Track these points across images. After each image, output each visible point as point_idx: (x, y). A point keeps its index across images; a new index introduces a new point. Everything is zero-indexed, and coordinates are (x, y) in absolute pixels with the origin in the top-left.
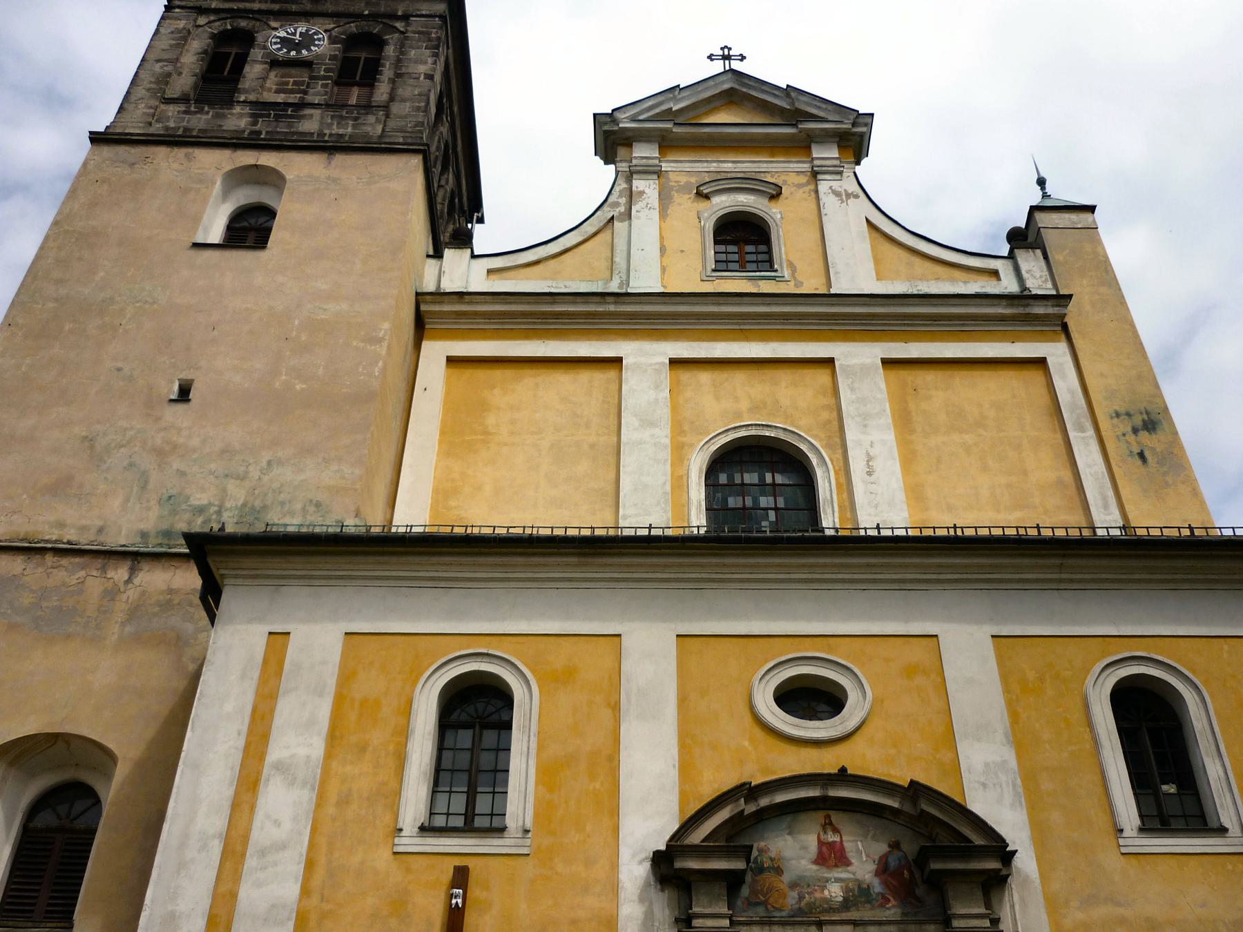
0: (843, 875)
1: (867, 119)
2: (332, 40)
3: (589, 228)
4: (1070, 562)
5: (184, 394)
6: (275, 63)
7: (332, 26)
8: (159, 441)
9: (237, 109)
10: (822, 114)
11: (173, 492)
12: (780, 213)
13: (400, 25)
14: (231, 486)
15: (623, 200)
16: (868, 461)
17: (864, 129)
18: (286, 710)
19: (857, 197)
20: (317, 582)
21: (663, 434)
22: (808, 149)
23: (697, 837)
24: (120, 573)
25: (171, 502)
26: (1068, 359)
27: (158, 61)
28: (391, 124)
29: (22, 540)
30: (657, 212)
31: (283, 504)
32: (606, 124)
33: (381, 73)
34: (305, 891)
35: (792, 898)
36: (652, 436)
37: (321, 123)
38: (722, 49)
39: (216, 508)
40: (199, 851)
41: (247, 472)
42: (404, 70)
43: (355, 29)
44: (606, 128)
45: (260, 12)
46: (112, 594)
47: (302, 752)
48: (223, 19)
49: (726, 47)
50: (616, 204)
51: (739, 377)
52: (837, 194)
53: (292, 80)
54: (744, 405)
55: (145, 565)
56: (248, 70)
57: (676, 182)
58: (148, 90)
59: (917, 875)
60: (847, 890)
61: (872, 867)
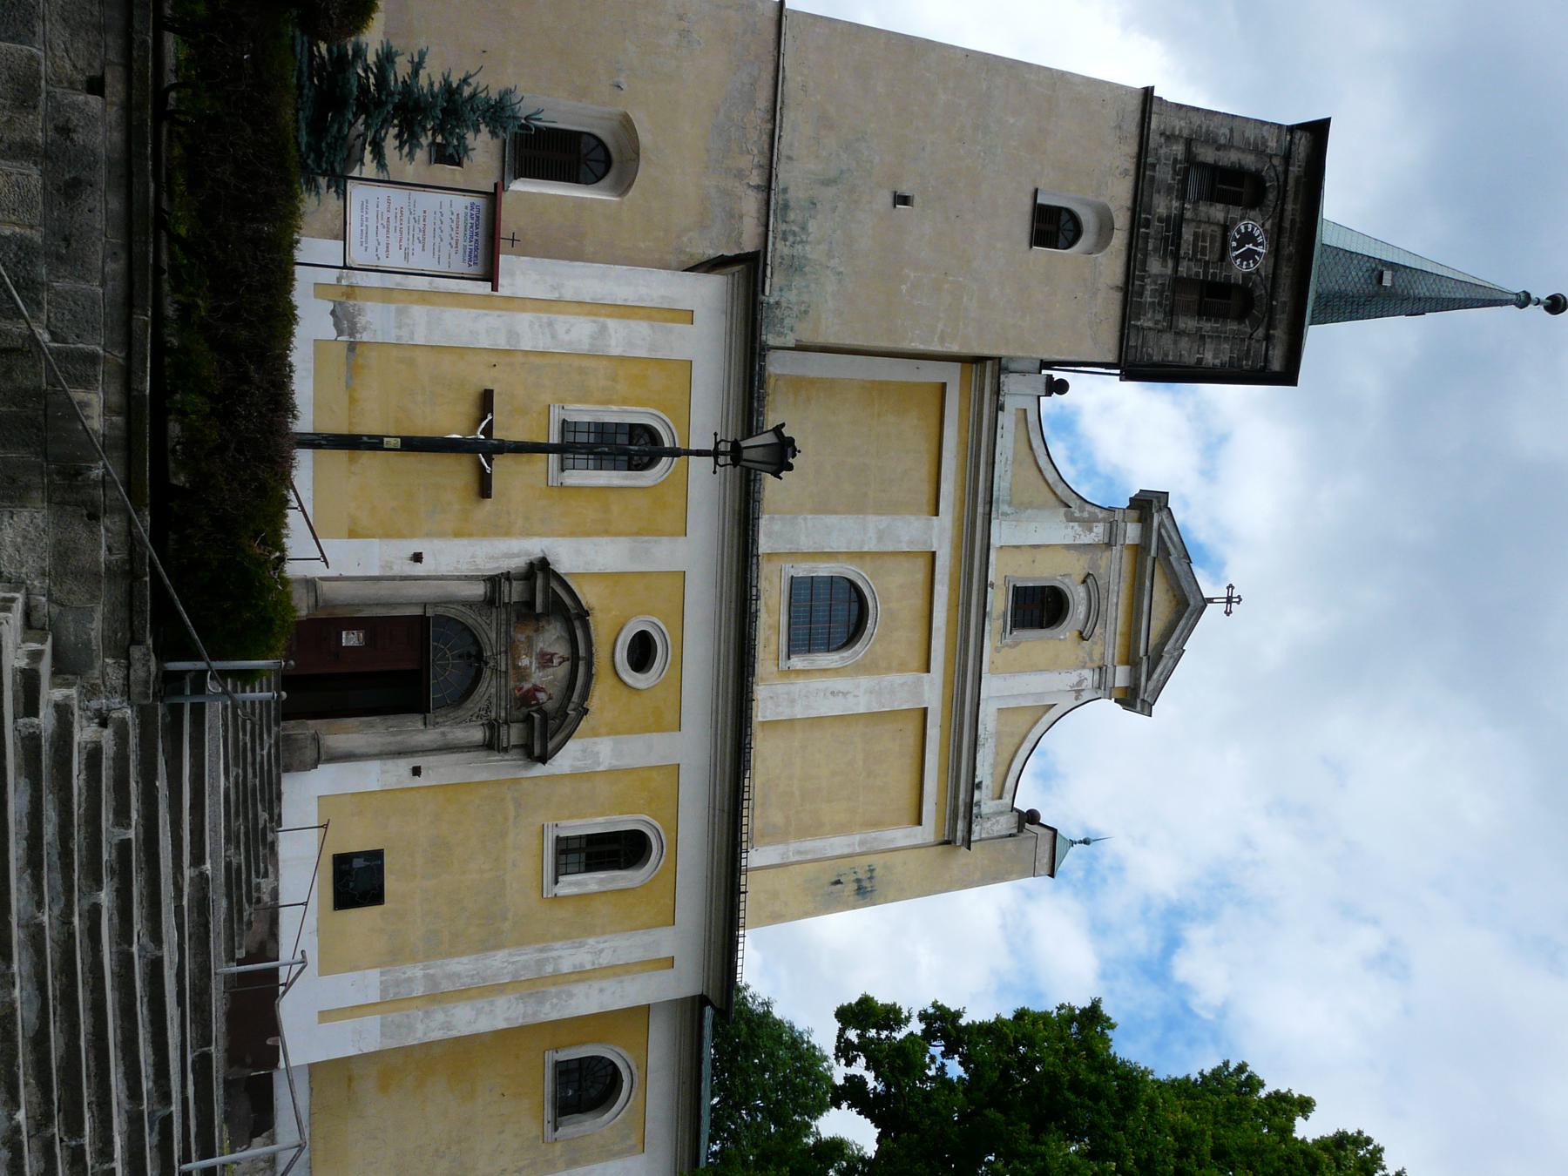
0: (533, 669)
1: (1147, 709)
2: (1246, 276)
3: (1060, 489)
4: (726, 815)
5: (902, 200)
6: (1226, 228)
7: (1263, 274)
9: (1175, 204)
10: (1155, 676)
12: (1065, 638)
13: (1260, 333)
15: (1086, 515)
17: (1139, 708)
18: (642, 328)
19: (1077, 699)
20: (728, 337)
21: (871, 546)
22: (1127, 663)
23: (554, 584)
24: (756, 178)
26: (919, 841)
27: (1231, 130)
28: (1151, 336)
29: (783, 102)
30: (1072, 542)
31: (807, 286)
32: (1159, 502)
33: (1208, 320)
34: (526, 352)
35: (521, 637)
37: (1156, 275)
38: (1239, 597)
40: (552, 286)
42: (1208, 340)
43: (1258, 294)
44: (1155, 502)
45: (1283, 211)
46: (740, 175)
47: (613, 342)
48: (1278, 179)
49: (1241, 600)
50: (1082, 510)
51: (919, 602)
52: (1080, 683)
53: (1208, 244)
55: (761, 196)
58: (1200, 127)
59: (534, 708)
60: (526, 668)
61: (538, 683)
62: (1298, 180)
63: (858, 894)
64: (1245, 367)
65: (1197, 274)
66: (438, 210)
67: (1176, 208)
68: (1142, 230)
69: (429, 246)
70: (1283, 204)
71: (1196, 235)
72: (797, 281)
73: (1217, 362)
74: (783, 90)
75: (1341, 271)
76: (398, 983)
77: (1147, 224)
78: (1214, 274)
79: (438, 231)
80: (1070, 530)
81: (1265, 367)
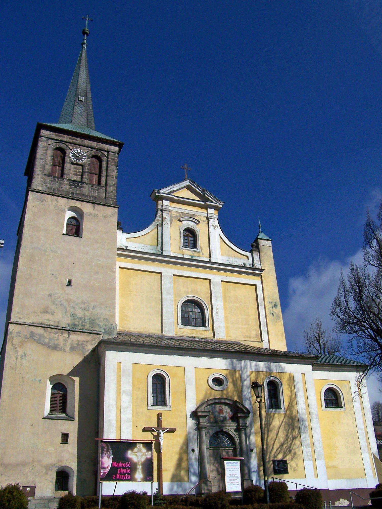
5: (69, 283)
7: (87, 151)
8: (67, 298)
9: (65, 182)
11: (73, 313)
12: (199, 230)
14: (86, 312)
15: (160, 219)
16: (217, 310)
25: (73, 316)
27: (41, 159)
36: (170, 297)
39: (84, 319)
41: (89, 309)
46: (65, 341)
53: (77, 170)
54: (190, 290)
56: (66, 166)
57: (174, 215)
58: (40, 171)
62: (57, 136)
63: (276, 307)
64: (118, 160)
65: (88, 175)
66: (228, 471)
67: (67, 182)
68: (75, 196)
69: (236, 473)
70: (64, 142)
71: (75, 175)
72: (97, 322)
73: (116, 171)
74: (30, 323)
75: (80, 116)
76: (308, 456)
77: (73, 193)
78: (88, 169)
79: (232, 471)
80: (165, 225)
81: (117, 153)
